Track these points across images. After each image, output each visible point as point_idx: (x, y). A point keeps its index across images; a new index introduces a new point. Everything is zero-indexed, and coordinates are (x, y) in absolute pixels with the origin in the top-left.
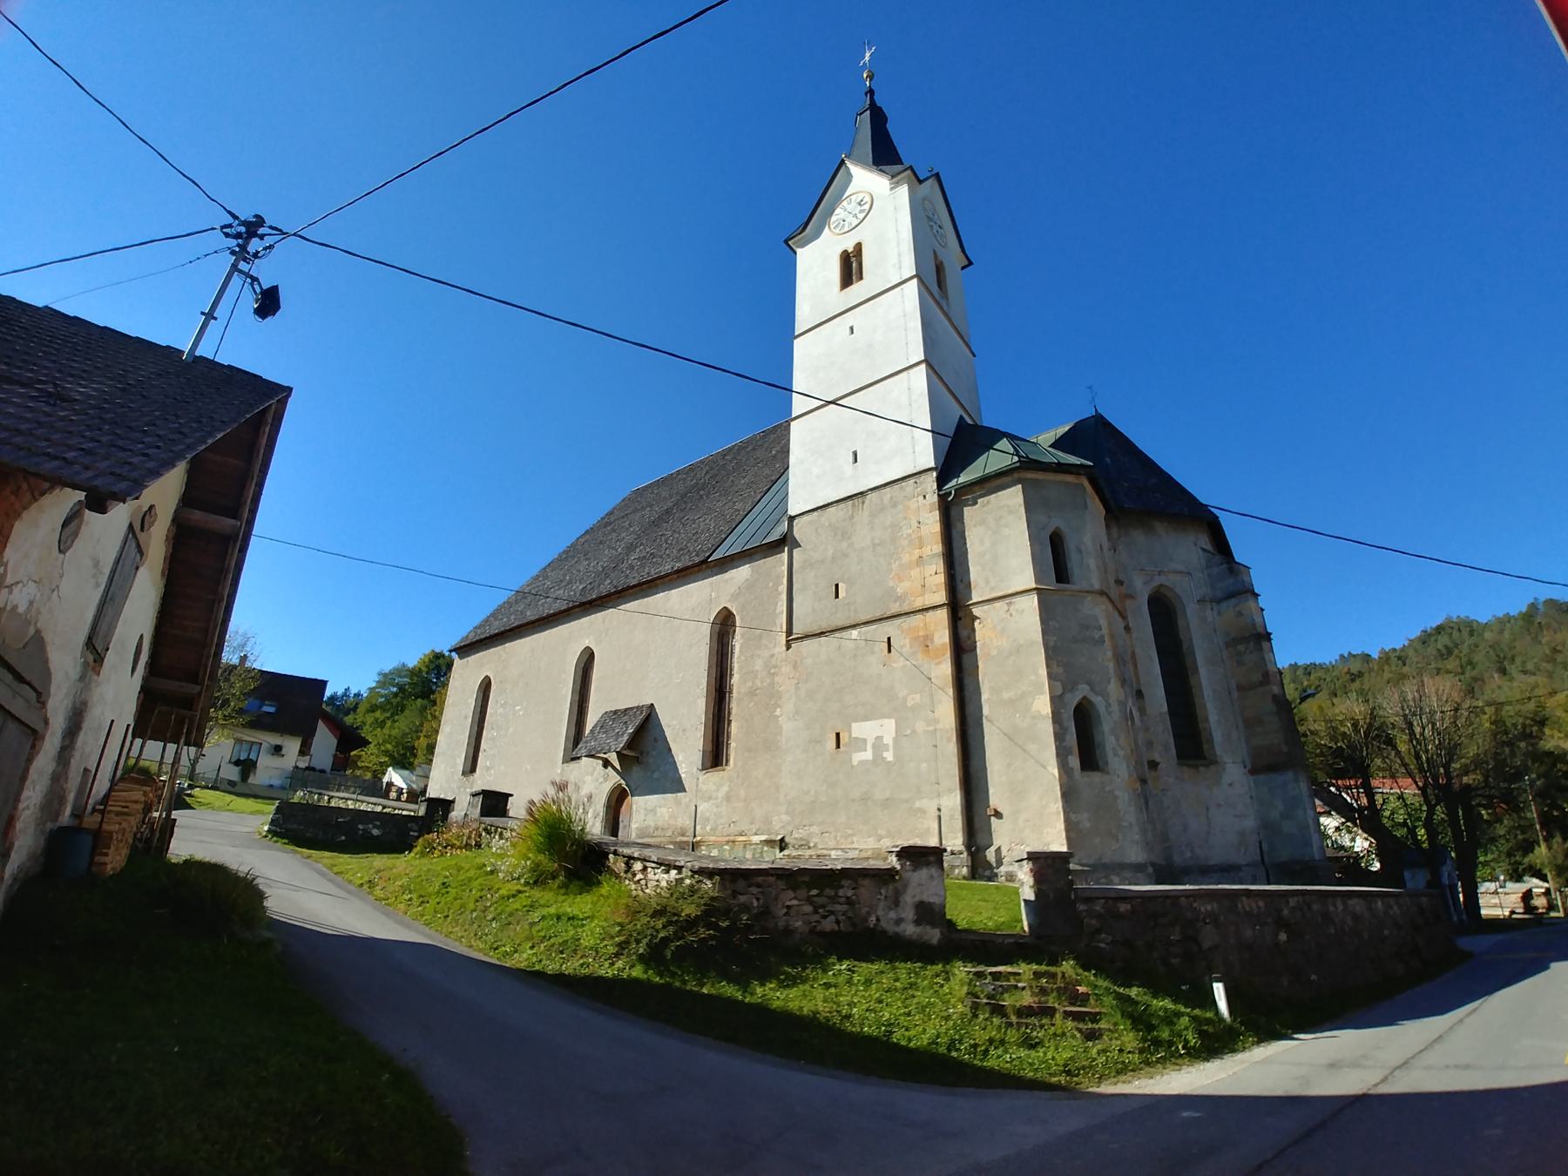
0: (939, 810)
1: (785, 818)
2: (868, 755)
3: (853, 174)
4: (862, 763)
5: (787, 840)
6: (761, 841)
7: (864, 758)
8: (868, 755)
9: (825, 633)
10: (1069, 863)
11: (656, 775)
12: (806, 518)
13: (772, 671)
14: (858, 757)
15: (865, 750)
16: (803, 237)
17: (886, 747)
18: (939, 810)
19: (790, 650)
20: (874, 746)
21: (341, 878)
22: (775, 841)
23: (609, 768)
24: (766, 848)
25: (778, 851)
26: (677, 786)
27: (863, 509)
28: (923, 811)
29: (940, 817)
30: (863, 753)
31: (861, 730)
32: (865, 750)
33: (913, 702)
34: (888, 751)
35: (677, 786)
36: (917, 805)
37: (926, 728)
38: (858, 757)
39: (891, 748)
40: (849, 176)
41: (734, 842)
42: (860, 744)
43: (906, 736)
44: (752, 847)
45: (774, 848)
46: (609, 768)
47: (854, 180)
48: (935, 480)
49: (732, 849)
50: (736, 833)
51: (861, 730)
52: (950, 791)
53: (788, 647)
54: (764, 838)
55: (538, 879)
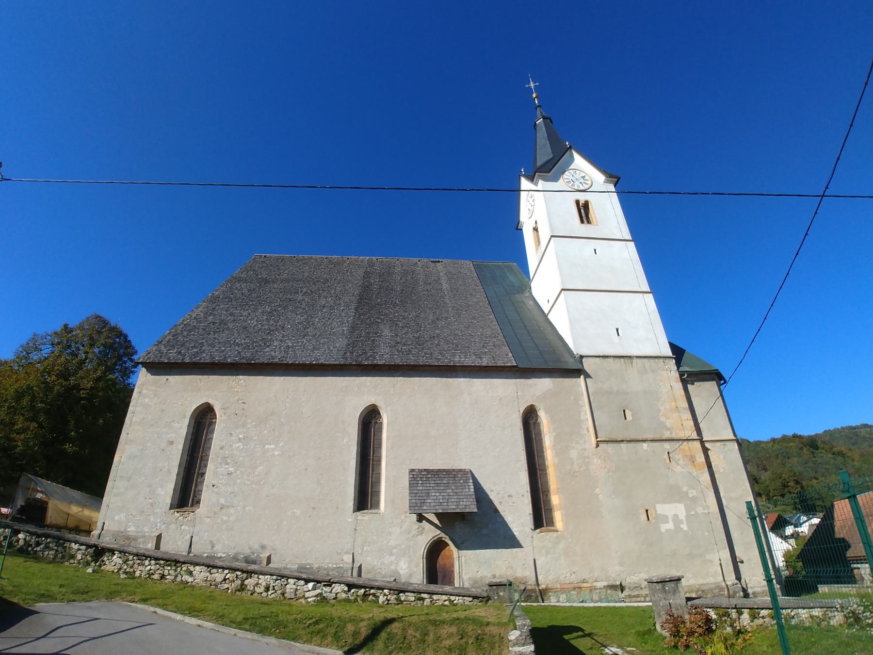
0: (720, 560)
1: (618, 568)
2: (670, 526)
3: (575, 158)
4: (668, 531)
5: (623, 584)
6: (604, 586)
7: (668, 528)
8: (670, 526)
9: (624, 441)
10: (780, 588)
11: (485, 531)
12: (590, 359)
13: (586, 460)
14: (664, 527)
15: (668, 523)
16: (546, 176)
17: (681, 522)
18: (720, 560)
19: (598, 448)
20: (673, 520)
21: (776, 634)
22: (616, 586)
23: (424, 521)
24: (609, 591)
25: (620, 593)
26: (510, 541)
27: (632, 367)
28: (711, 561)
29: (721, 564)
30: (667, 524)
31: (663, 509)
32: (668, 523)
33: (692, 495)
34: (683, 523)
35: (510, 541)
36: (707, 557)
37: (703, 511)
38: (664, 527)
39: (685, 522)
40: (572, 159)
41: (580, 588)
42: (665, 519)
43: (692, 515)
44: (597, 591)
45: (617, 590)
46: (424, 521)
47: (575, 161)
48: (674, 364)
49: (579, 593)
50: (579, 581)
51: (663, 509)
52: (724, 549)
53: (597, 446)
54: (606, 584)
55: (139, 556)
